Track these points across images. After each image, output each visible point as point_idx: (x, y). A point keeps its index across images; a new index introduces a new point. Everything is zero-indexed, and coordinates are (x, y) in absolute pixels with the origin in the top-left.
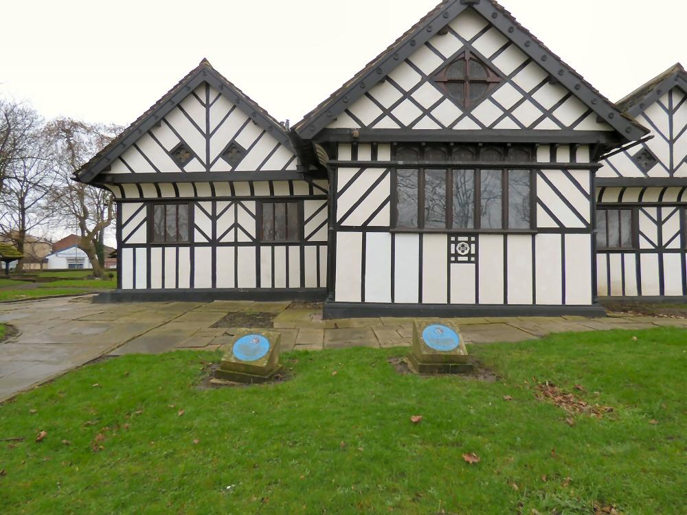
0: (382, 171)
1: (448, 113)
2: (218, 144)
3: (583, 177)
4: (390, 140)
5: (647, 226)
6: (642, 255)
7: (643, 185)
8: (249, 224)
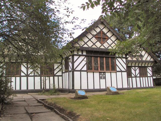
0: (84, 57)
1: (98, 44)
3: (124, 60)
4: (82, 49)
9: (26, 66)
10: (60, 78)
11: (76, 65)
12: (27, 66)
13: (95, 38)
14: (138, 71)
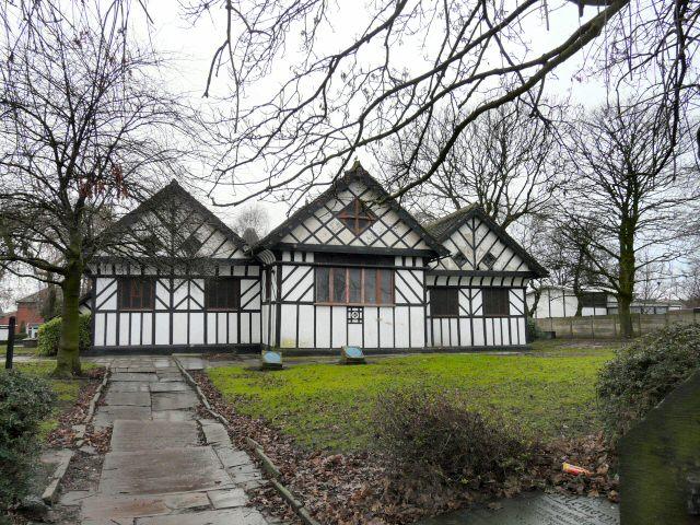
1: (347, 237)
2: (480, 254)
5: (463, 301)
6: (157, 314)
7: (461, 274)
8: (200, 297)
9: (168, 286)
10: (256, 316)
11: (285, 288)
12: (172, 286)
13: (339, 219)
14: (478, 301)
